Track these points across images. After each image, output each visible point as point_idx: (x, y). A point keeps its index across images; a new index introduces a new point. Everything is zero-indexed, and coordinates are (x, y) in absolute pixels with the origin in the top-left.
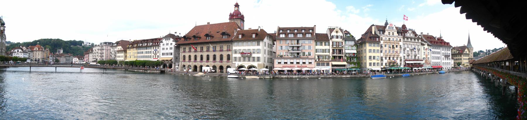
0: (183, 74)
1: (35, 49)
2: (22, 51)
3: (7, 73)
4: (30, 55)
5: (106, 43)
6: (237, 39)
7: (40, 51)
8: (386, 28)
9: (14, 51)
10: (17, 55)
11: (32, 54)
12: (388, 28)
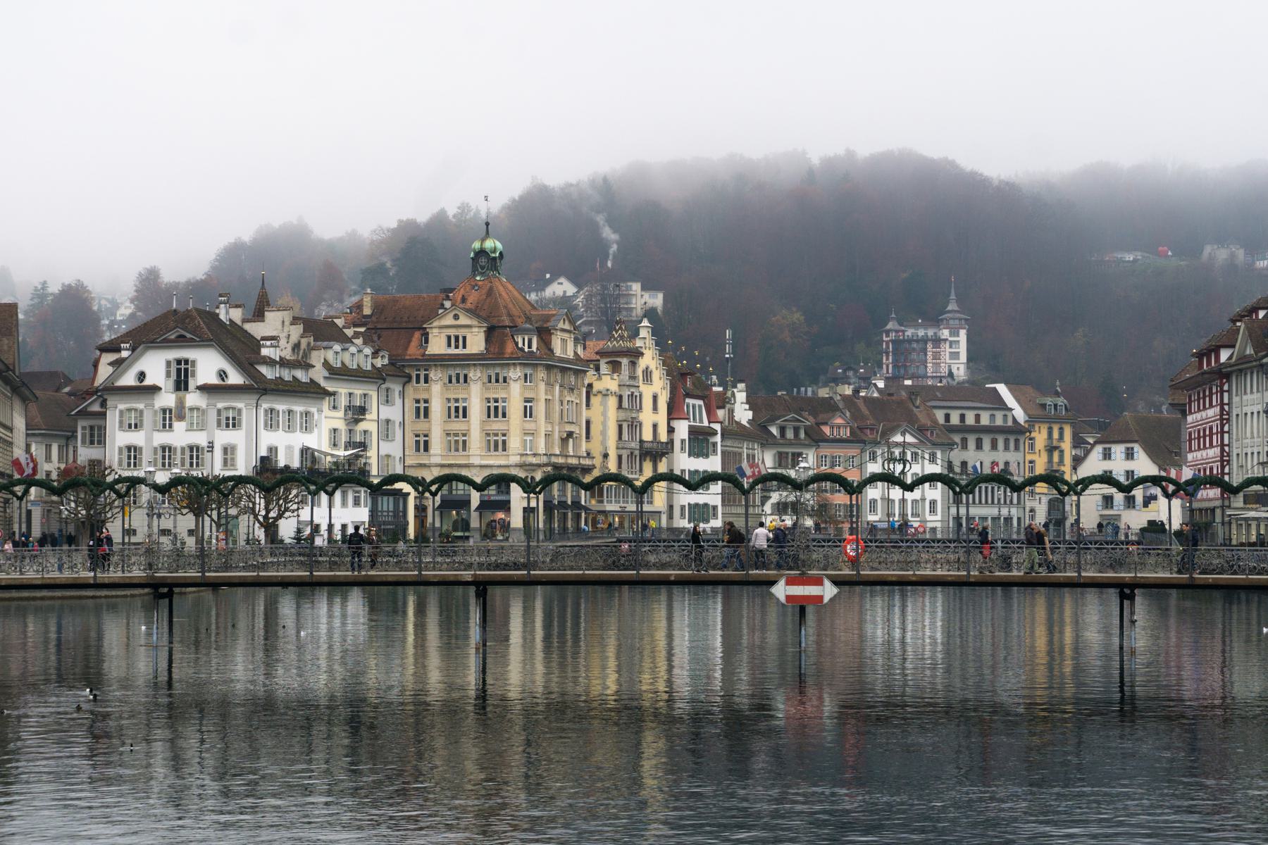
0: (920, 321)
1: (437, 346)
2: (235, 378)
4: (369, 424)
9: (129, 379)
10: (167, 426)
11: (393, 412)
12: (952, 365)
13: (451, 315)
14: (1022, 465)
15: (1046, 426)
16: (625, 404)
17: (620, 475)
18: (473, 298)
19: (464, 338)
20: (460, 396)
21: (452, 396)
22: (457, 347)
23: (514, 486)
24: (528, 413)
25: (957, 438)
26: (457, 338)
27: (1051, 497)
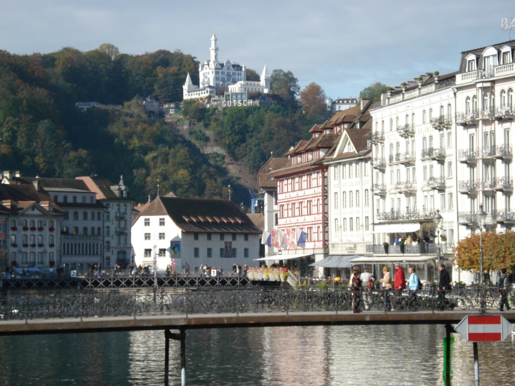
14: (102, 230)
15: (116, 204)
23: (26, 155)
25: (71, 212)
27: (119, 250)
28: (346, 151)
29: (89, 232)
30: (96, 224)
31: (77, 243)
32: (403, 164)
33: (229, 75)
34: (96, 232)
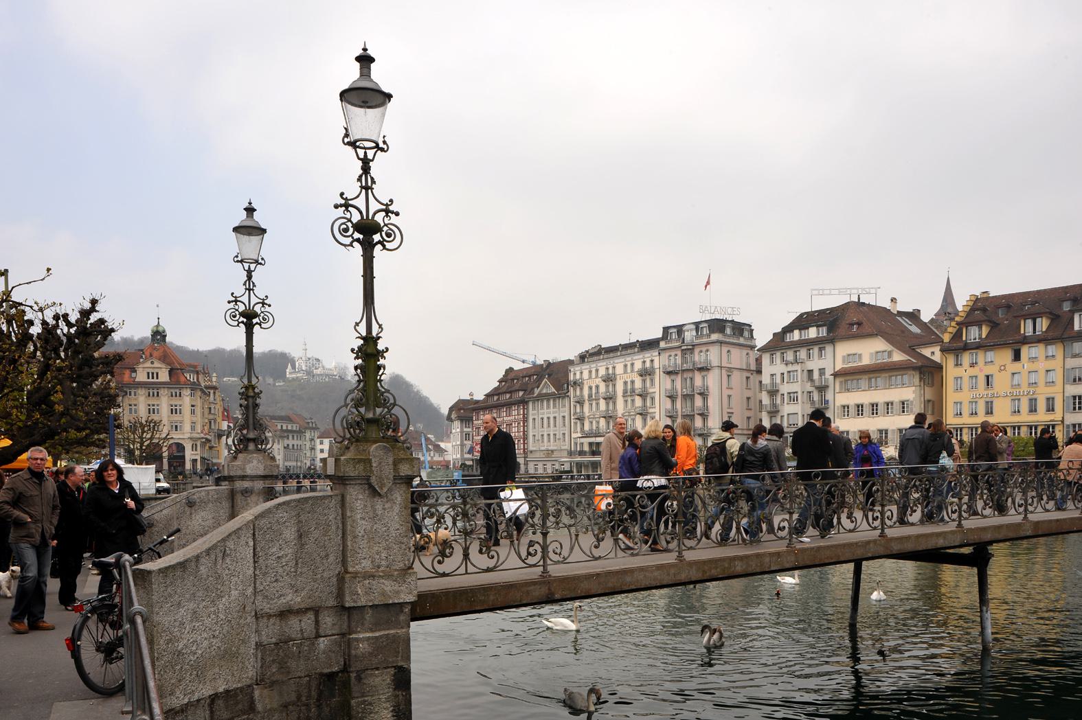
1: (141, 376)
3: (349, 486)
5: (717, 325)
6: (783, 344)
7: (186, 392)
8: (347, 104)
13: (150, 362)
16: (212, 412)
17: (730, 421)
18: (156, 354)
19: (157, 374)
20: (155, 403)
21: (151, 403)
22: (153, 378)
24: (193, 412)
26: (153, 374)
28: (544, 391)
29: (295, 447)
30: (299, 442)
31: (552, 417)
32: (638, 395)
33: (313, 364)
34: (299, 448)
